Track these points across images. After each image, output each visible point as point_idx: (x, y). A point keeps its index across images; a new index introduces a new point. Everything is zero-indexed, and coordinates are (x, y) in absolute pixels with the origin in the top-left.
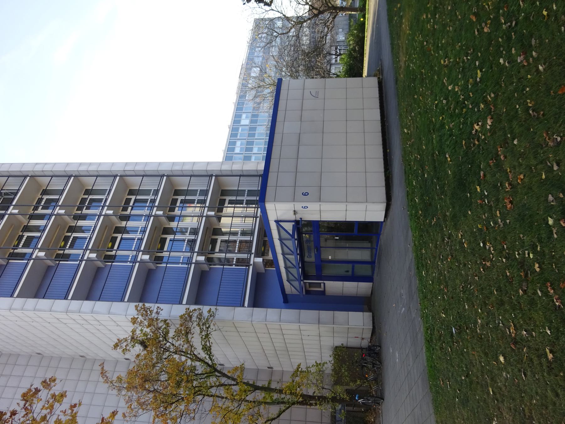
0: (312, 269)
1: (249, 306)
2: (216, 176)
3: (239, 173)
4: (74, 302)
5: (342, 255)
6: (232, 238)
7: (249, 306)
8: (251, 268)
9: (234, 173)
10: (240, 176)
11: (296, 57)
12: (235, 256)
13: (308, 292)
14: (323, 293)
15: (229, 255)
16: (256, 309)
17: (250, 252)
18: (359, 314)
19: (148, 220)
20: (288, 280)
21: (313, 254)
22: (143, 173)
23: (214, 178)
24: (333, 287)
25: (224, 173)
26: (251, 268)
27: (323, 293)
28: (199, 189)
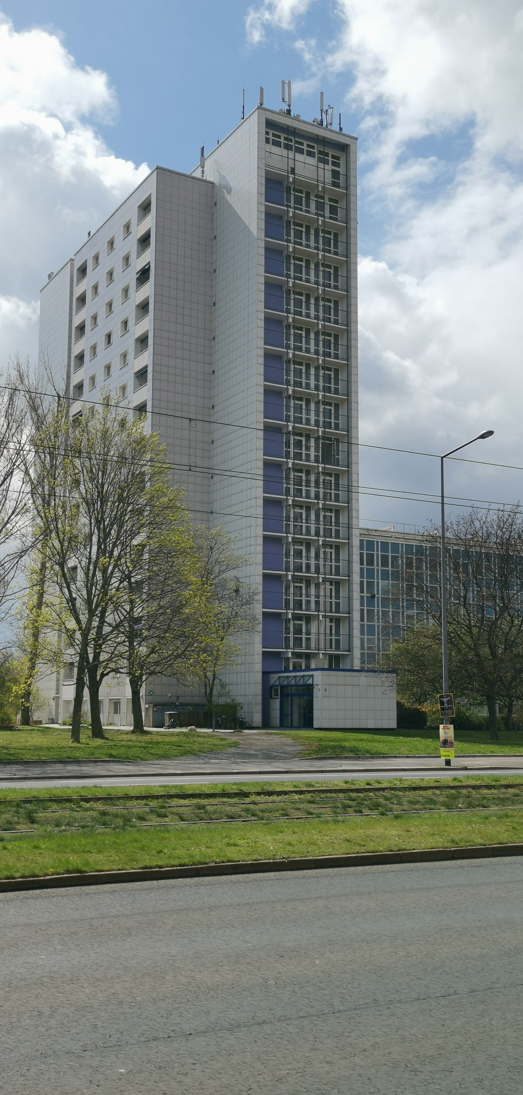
0: (285, 692)
1: (264, 421)
2: (349, 579)
3: (350, 560)
4: (263, 242)
5: (296, 709)
6: (304, 411)
7: (263, 652)
8: (285, 650)
9: (351, 630)
10: (349, 561)
11: (484, 492)
12: (292, 414)
13: (271, 687)
14: (271, 698)
15: (292, 409)
16: (262, 539)
17: (294, 609)
18: (260, 720)
19: (315, 319)
20: (279, 677)
21: (295, 692)
22: (349, 311)
23: (347, 578)
24: (276, 704)
25: (351, 623)
26: (285, 650)
27: (271, 698)
28: (339, 352)
